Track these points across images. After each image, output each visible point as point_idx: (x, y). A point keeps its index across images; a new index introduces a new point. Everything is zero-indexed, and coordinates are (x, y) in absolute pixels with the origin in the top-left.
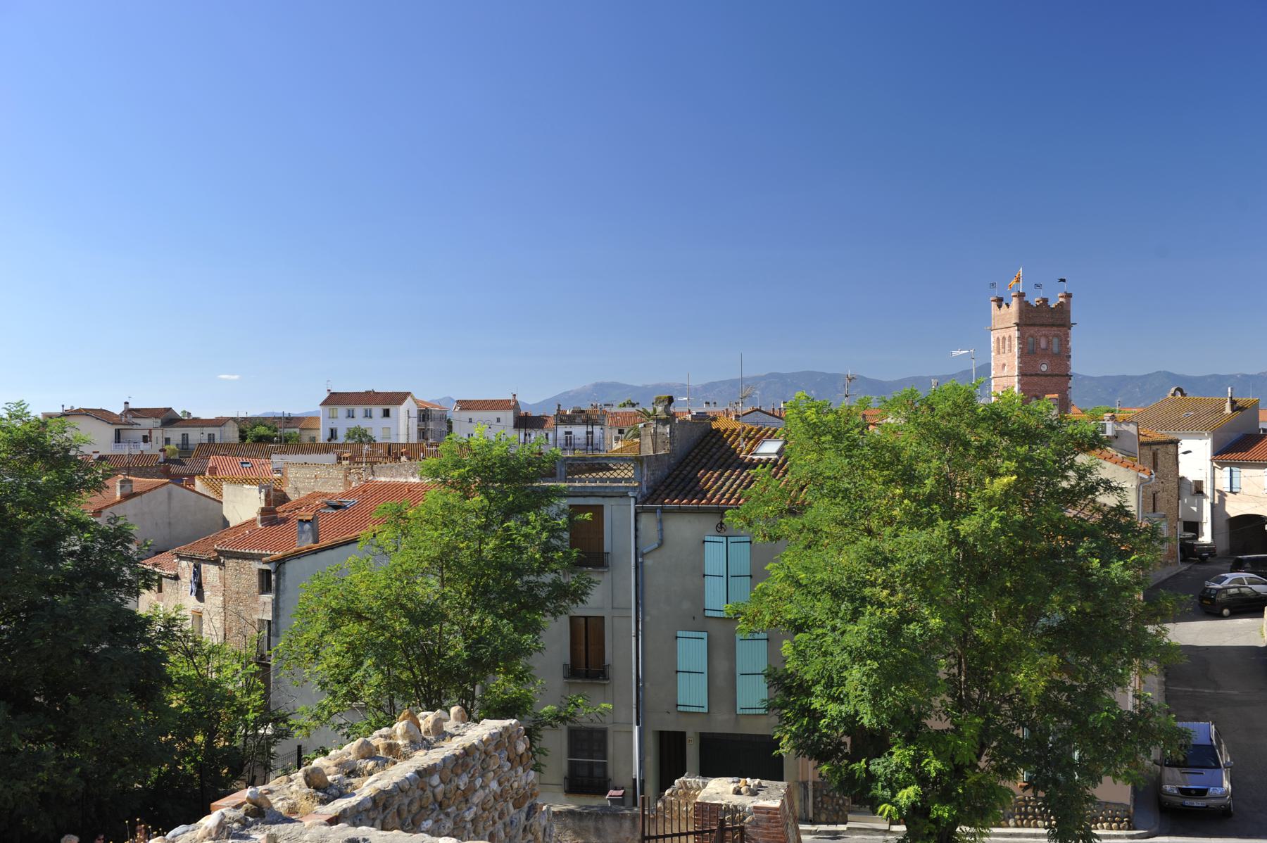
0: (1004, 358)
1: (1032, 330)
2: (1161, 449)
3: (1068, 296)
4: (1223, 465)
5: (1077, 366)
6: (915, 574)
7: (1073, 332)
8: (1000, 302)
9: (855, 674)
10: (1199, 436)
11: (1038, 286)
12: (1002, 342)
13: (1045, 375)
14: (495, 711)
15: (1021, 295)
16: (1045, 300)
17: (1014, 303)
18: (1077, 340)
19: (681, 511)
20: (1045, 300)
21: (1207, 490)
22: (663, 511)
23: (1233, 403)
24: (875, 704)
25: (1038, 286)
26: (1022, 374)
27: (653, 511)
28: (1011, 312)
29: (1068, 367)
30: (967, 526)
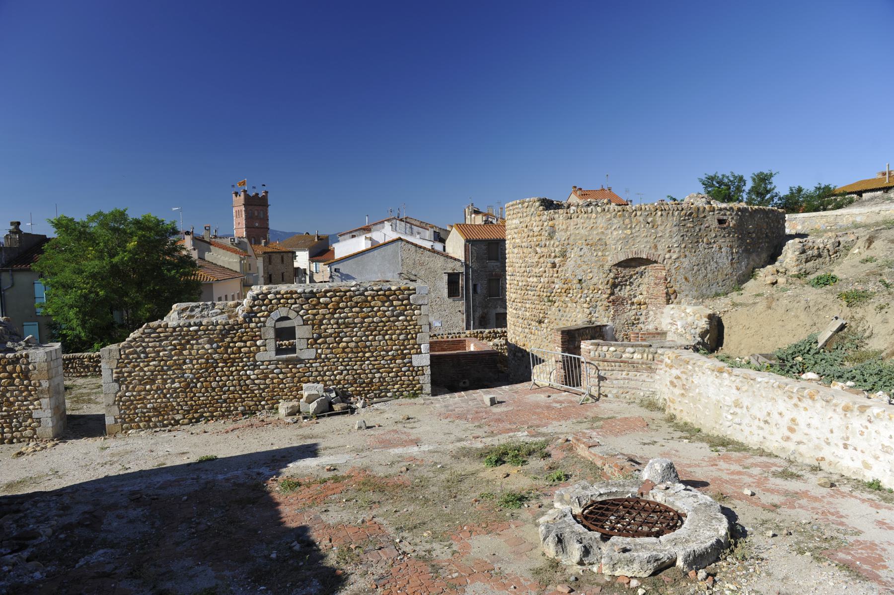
0: (239, 220)
1: (250, 207)
2: (285, 256)
3: (266, 192)
4: (313, 262)
5: (273, 225)
6: (93, 276)
7: (269, 208)
8: (236, 194)
9: (71, 314)
10: (305, 250)
11: (254, 187)
12: (238, 212)
13: (257, 228)
14: (77, 490)
15: (245, 191)
16: (257, 194)
17: (242, 194)
18: (271, 212)
19: (21, 270)
20: (257, 194)
21: (308, 272)
22: (12, 271)
23: (318, 237)
24: (84, 327)
25: (254, 187)
26: (247, 227)
27: (7, 271)
28: (242, 198)
29: (268, 224)
30: (116, 260)
